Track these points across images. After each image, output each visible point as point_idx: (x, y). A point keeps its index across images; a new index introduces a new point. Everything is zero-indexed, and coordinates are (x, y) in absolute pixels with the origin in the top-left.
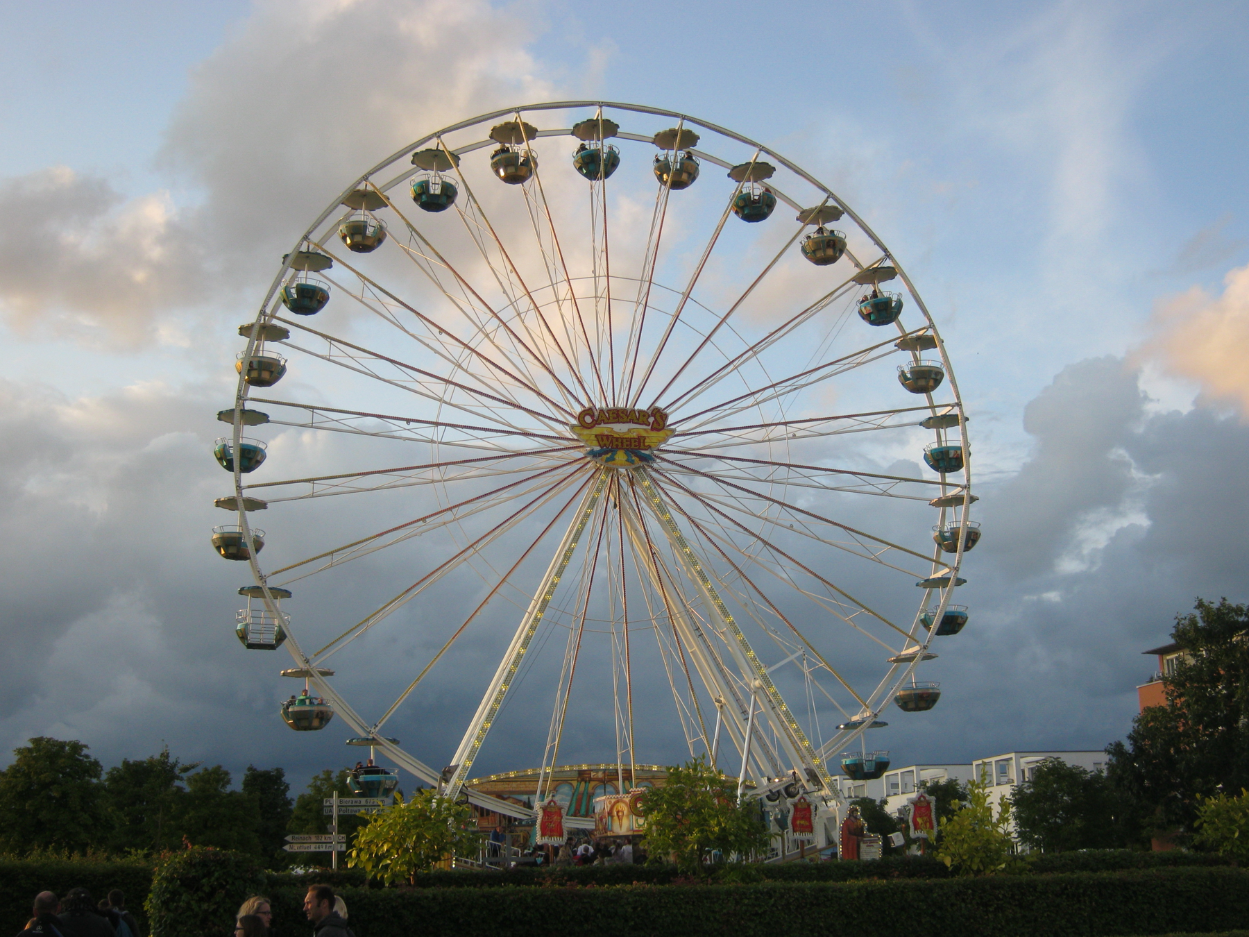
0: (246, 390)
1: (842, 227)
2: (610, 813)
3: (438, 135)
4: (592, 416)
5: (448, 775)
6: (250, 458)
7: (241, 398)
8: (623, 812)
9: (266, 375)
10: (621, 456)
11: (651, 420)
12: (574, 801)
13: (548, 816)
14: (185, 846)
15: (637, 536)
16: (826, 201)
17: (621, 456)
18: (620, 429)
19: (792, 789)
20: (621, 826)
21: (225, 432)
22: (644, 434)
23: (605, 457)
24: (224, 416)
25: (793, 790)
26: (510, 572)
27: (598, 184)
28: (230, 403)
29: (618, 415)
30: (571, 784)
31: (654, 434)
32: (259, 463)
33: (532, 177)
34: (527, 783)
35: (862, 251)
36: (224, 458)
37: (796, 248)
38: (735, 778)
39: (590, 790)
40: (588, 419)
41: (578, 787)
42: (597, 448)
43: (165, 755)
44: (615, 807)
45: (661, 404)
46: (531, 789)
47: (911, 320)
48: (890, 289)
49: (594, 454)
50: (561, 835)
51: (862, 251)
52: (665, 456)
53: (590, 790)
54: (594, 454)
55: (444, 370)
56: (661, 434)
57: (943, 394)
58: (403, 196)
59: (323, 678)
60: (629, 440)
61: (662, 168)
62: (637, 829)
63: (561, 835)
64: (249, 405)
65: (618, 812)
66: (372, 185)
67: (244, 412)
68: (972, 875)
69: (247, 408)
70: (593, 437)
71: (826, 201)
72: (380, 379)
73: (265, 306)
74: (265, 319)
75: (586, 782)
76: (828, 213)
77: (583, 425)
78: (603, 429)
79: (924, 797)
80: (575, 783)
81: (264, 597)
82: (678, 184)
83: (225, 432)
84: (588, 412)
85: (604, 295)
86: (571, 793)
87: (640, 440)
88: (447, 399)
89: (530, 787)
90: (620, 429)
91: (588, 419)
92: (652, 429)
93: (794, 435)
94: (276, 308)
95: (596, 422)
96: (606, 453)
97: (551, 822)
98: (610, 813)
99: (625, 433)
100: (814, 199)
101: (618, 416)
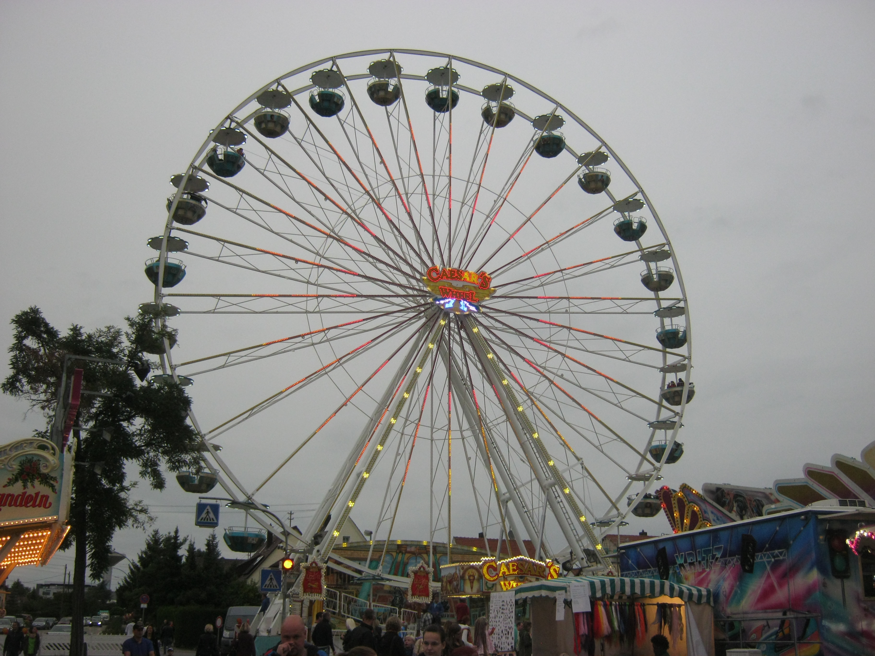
0: (172, 223)
1: (608, 167)
2: (463, 577)
3: (333, 59)
5: (319, 539)
6: (174, 275)
7: (169, 228)
8: (474, 576)
9: (189, 214)
12: (393, 567)
13: (418, 579)
15: (494, 343)
16: (600, 148)
19: (568, 565)
20: (472, 588)
21: (154, 255)
24: (155, 243)
25: (569, 565)
26: (545, 203)
27: (441, 116)
28: (159, 231)
30: (392, 554)
31: (481, 291)
32: (179, 281)
33: (395, 103)
34: (359, 552)
35: (620, 188)
36: (151, 273)
37: (575, 179)
39: (405, 559)
44: (467, 573)
45: (487, 269)
46: (362, 556)
47: (651, 239)
48: (636, 216)
50: (427, 595)
51: (620, 188)
53: (405, 559)
55: (301, 289)
57: (673, 291)
61: (487, 115)
62: (486, 591)
63: (427, 595)
64: (174, 233)
65: (469, 576)
66: (283, 87)
67: (171, 240)
68: (653, 631)
69: (172, 235)
70: (437, 288)
71: (600, 148)
72: (257, 313)
73: (194, 161)
74: (192, 171)
75: (402, 554)
76: (598, 157)
77: (431, 280)
79: (424, 568)
80: (394, 554)
81: (166, 262)
82: (501, 123)
83: (154, 255)
85: (444, 193)
86: (391, 562)
88: (312, 280)
89: (361, 554)
93: (567, 311)
94: (202, 164)
97: (420, 584)
98: (463, 577)
99: (460, 288)
100: (590, 146)
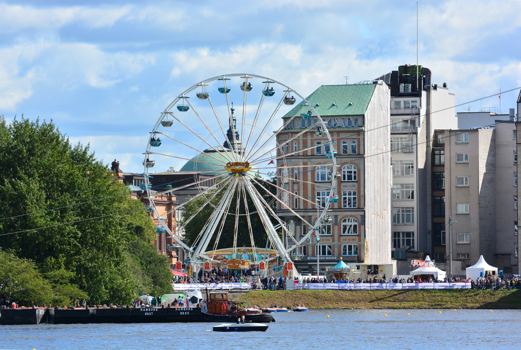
4: (230, 164)
10: (237, 174)
11: (245, 165)
14: (30, 75)
17: (237, 174)
18: (237, 168)
22: (243, 168)
23: (233, 175)
29: (237, 164)
31: (246, 168)
38: (441, 197)
40: (229, 165)
41: (238, 253)
42: (231, 173)
43: (51, 127)
49: (230, 174)
52: (249, 175)
53: (241, 254)
54: (230, 174)
56: (248, 168)
58: (174, 109)
59: (221, 153)
60: (239, 170)
78: (233, 168)
84: (229, 163)
87: (242, 170)
90: (237, 168)
91: (229, 165)
92: (245, 167)
95: (231, 166)
96: (233, 174)
101: (237, 164)
